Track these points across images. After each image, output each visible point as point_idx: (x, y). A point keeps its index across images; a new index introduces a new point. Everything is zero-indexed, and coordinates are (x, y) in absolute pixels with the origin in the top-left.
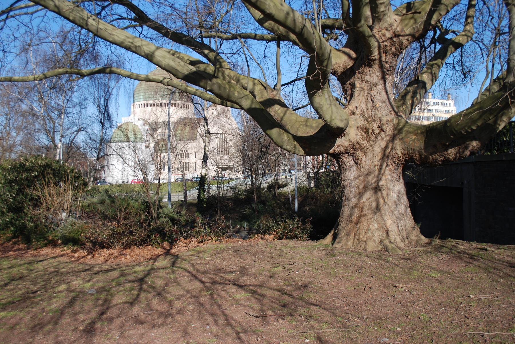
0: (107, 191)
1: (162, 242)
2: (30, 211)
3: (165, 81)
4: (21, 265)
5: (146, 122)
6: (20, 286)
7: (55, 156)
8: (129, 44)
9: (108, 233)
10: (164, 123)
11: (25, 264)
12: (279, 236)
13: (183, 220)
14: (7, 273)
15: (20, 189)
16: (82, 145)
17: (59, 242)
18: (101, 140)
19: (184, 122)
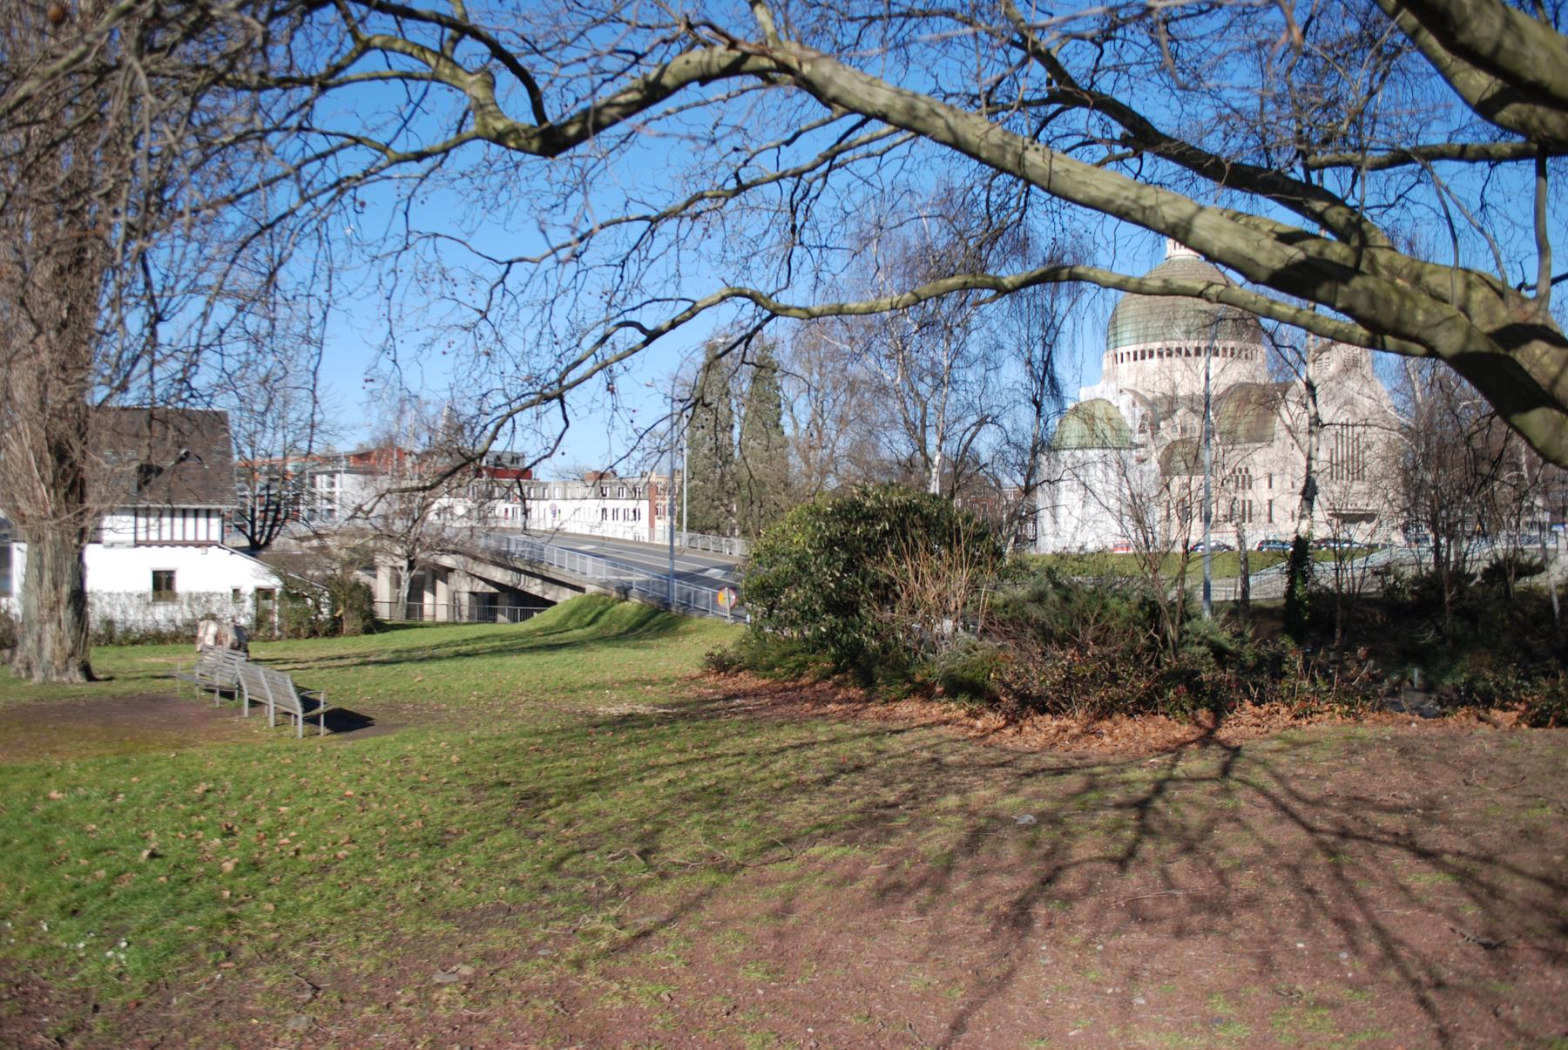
0: (1050, 572)
1: (1194, 708)
2: (872, 614)
3: (1212, 290)
4: (855, 737)
5: (1138, 398)
6: (857, 788)
7: (924, 484)
8: (1127, 203)
9: (1058, 676)
10: (1191, 398)
11: (864, 735)
12: (1535, 716)
13: (1249, 655)
14: (827, 755)
15: (849, 561)
16: (985, 457)
17: (939, 689)
18: (1035, 446)
19: (1241, 393)
